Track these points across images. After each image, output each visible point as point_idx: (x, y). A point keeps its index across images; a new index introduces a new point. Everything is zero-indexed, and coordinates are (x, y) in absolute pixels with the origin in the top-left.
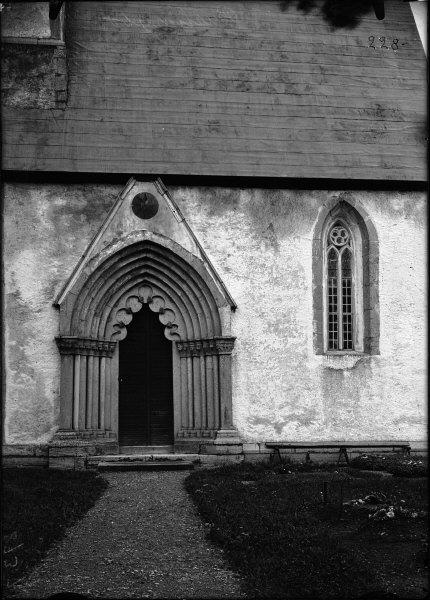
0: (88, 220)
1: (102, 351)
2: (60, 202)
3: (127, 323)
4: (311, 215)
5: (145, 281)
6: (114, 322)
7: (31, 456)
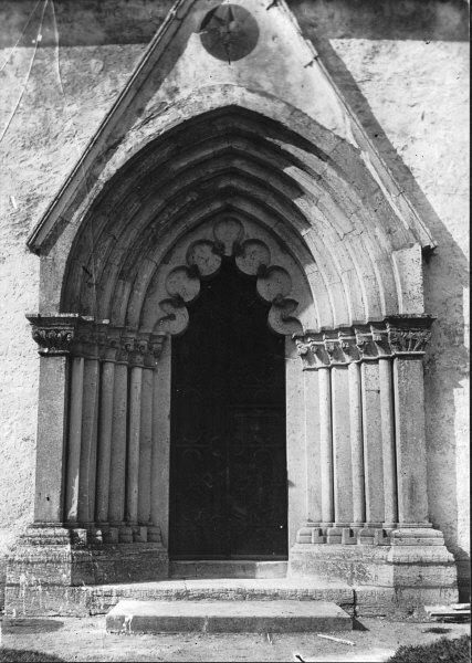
6: (161, 294)
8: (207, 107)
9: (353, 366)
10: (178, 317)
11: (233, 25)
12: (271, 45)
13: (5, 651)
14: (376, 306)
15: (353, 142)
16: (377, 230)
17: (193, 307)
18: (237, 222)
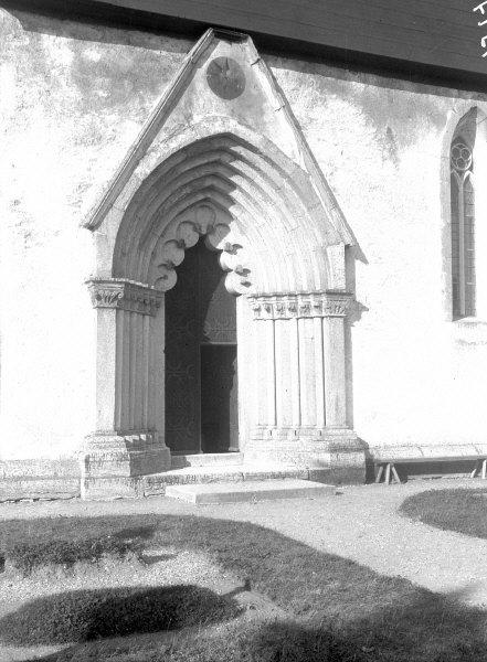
0: (135, 90)
2: (94, 52)
3: (177, 264)
4: (438, 120)
5: (206, 200)
6: (160, 261)
7: (49, 478)
8: (212, 133)
9: (294, 320)
10: (170, 277)
11: (228, 73)
12: (254, 92)
13: (480, 534)
14: (311, 281)
15: (304, 168)
16: (316, 230)
17: (179, 269)
18: (210, 208)
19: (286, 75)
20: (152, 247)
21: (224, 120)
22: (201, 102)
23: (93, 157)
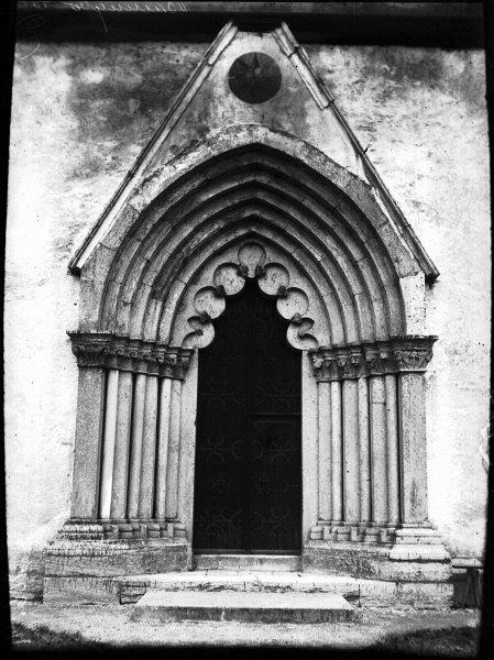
1: (162, 363)
5: (251, 235)
6: (190, 312)
11: (258, 71)
17: (218, 323)
19: (338, 63)
20: (176, 296)
21: (251, 127)
22: (220, 110)
23: (87, 192)
